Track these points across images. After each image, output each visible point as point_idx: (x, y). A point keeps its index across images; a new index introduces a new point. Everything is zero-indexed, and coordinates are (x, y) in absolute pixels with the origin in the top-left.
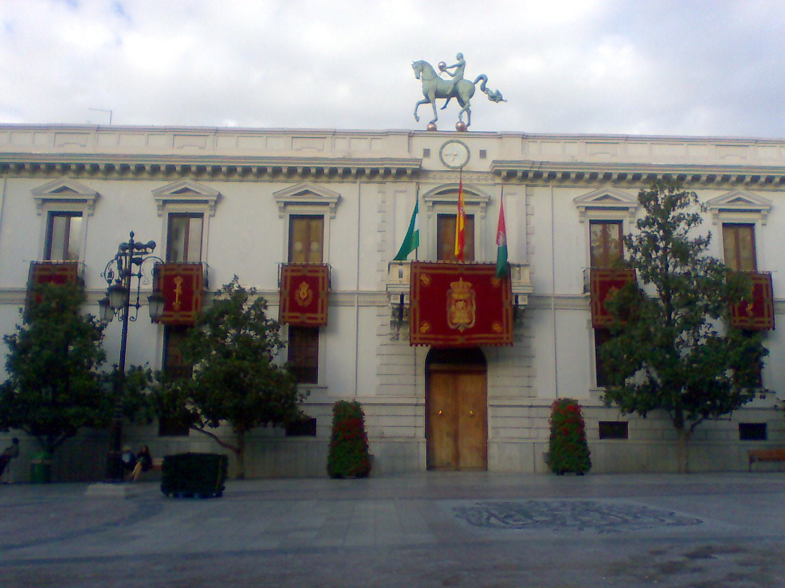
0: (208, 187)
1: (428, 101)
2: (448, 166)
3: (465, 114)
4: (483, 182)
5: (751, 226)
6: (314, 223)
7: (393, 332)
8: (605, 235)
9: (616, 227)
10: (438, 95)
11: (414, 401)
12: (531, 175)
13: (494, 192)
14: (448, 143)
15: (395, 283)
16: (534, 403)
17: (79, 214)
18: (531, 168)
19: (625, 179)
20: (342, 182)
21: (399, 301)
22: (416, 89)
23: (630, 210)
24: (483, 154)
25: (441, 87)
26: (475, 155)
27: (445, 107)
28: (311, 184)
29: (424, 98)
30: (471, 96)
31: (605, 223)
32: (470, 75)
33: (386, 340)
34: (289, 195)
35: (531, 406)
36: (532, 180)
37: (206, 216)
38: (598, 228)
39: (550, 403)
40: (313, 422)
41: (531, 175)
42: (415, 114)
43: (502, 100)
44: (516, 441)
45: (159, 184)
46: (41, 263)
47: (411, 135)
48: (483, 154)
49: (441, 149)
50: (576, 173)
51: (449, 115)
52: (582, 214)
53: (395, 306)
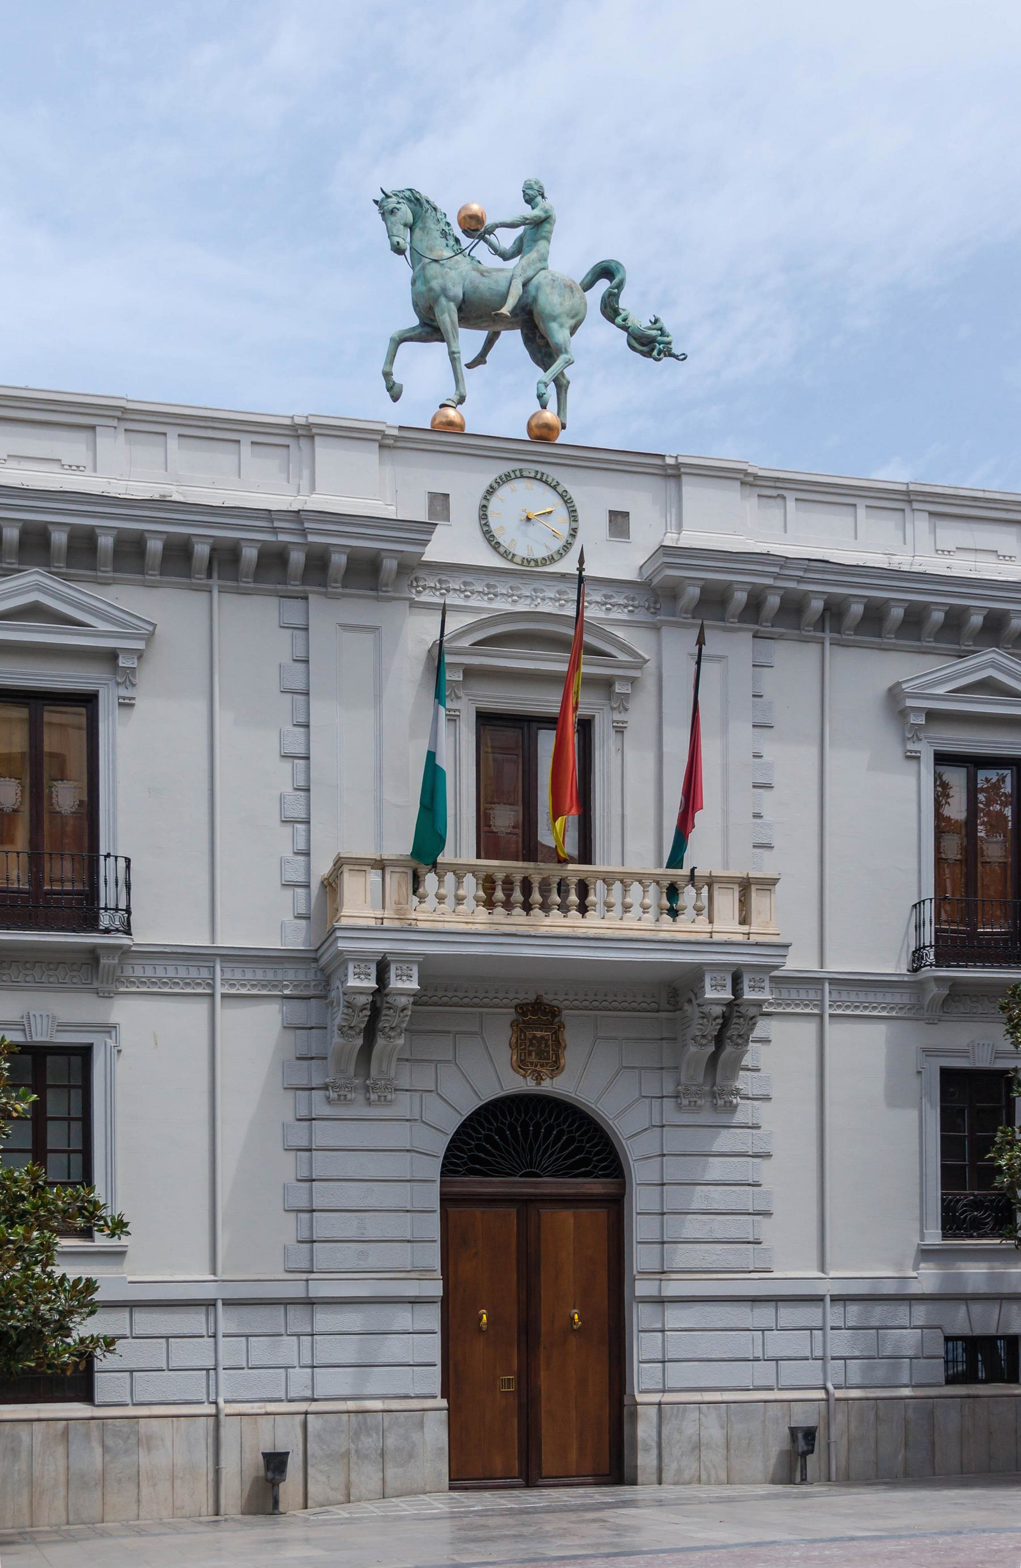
0: (110, 607)
1: (429, 330)
2: (506, 555)
5: (88, 701)
9: (77, 716)
12: (774, 601)
24: (619, 522)
27: (480, 359)
30: (573, 330)
31: (974, 763)
32: (567, 257)
36: (820, 624)
38: (957, 778)
42: (387, 375)
46: (965, 870)
48: (619, 522)
49: (485, 498)
50: (985, 612)
51: (503, 393)
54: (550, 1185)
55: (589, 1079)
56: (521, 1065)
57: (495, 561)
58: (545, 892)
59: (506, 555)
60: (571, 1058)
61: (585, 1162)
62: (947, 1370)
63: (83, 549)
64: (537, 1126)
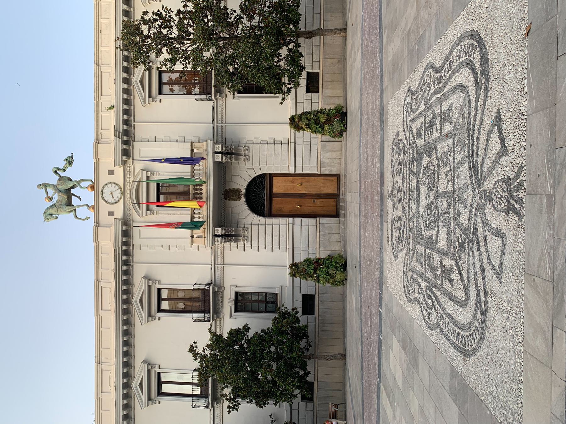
0: (139, 287)
3: (82, 184)
4: (131, 168)
6: (163, 190)
7: (242, 240)
8: (171, 83)
10: (69, 204)
11: (291, 226)
12: (125, 138)
13: (139, 166)
14: (103, 199)
15: (206, 241)
16: (293, 140)
17: (159, 374)
18: (119, 138)
19: (127, 100)
20: (133, 275)
21: (220, 239)
22: (65, 217)
23: (150, 369)
24: (111, 173)
25: (64, 202)
26: (111, 178)
28: (135, 297)
29: (72, 214)
30: (70, 180)
31: (161, 84)
33: (248, 245)
34: (143, 398)
35: (295, 143)
37: (159, 371)
38: (166, 89)
39: (293, 131)
40: (305, 297)
41: (125, 138)
43: (72, 157)
44: (319, 151)
45: (137, 321)
47: (98, 225)
48: (111, 173)
51: (84, 196)
52: (154, 100)
53: (134, 224)
54: (267, 191)
55: (241, 182)
56: (239, 199)
57: (122, 201)
58: (197, 189)
59: (120, 199)
60: (237, 187)
61: (262, 182)
62: (344, 292)
63: (127, 375)
64: (253, 193)
